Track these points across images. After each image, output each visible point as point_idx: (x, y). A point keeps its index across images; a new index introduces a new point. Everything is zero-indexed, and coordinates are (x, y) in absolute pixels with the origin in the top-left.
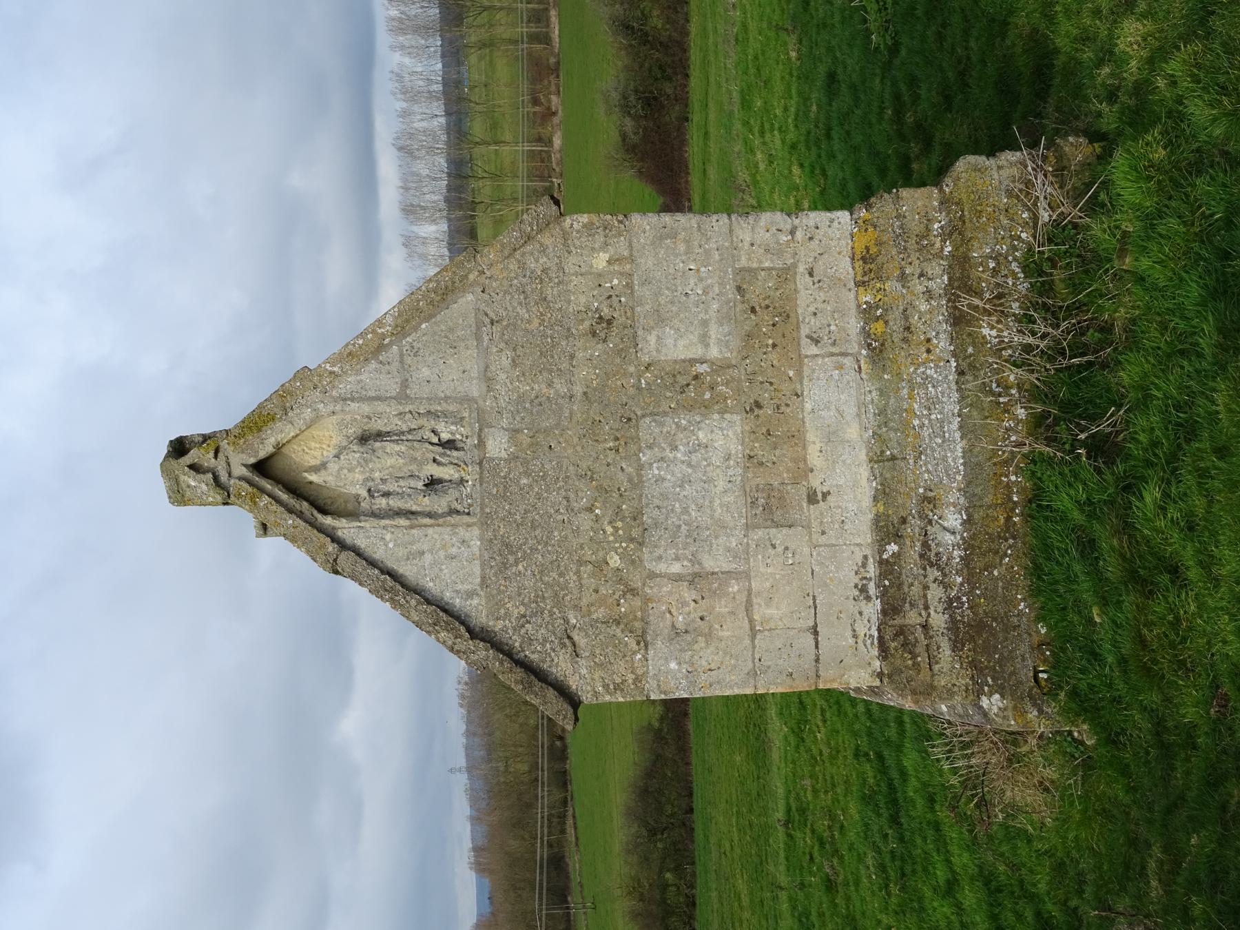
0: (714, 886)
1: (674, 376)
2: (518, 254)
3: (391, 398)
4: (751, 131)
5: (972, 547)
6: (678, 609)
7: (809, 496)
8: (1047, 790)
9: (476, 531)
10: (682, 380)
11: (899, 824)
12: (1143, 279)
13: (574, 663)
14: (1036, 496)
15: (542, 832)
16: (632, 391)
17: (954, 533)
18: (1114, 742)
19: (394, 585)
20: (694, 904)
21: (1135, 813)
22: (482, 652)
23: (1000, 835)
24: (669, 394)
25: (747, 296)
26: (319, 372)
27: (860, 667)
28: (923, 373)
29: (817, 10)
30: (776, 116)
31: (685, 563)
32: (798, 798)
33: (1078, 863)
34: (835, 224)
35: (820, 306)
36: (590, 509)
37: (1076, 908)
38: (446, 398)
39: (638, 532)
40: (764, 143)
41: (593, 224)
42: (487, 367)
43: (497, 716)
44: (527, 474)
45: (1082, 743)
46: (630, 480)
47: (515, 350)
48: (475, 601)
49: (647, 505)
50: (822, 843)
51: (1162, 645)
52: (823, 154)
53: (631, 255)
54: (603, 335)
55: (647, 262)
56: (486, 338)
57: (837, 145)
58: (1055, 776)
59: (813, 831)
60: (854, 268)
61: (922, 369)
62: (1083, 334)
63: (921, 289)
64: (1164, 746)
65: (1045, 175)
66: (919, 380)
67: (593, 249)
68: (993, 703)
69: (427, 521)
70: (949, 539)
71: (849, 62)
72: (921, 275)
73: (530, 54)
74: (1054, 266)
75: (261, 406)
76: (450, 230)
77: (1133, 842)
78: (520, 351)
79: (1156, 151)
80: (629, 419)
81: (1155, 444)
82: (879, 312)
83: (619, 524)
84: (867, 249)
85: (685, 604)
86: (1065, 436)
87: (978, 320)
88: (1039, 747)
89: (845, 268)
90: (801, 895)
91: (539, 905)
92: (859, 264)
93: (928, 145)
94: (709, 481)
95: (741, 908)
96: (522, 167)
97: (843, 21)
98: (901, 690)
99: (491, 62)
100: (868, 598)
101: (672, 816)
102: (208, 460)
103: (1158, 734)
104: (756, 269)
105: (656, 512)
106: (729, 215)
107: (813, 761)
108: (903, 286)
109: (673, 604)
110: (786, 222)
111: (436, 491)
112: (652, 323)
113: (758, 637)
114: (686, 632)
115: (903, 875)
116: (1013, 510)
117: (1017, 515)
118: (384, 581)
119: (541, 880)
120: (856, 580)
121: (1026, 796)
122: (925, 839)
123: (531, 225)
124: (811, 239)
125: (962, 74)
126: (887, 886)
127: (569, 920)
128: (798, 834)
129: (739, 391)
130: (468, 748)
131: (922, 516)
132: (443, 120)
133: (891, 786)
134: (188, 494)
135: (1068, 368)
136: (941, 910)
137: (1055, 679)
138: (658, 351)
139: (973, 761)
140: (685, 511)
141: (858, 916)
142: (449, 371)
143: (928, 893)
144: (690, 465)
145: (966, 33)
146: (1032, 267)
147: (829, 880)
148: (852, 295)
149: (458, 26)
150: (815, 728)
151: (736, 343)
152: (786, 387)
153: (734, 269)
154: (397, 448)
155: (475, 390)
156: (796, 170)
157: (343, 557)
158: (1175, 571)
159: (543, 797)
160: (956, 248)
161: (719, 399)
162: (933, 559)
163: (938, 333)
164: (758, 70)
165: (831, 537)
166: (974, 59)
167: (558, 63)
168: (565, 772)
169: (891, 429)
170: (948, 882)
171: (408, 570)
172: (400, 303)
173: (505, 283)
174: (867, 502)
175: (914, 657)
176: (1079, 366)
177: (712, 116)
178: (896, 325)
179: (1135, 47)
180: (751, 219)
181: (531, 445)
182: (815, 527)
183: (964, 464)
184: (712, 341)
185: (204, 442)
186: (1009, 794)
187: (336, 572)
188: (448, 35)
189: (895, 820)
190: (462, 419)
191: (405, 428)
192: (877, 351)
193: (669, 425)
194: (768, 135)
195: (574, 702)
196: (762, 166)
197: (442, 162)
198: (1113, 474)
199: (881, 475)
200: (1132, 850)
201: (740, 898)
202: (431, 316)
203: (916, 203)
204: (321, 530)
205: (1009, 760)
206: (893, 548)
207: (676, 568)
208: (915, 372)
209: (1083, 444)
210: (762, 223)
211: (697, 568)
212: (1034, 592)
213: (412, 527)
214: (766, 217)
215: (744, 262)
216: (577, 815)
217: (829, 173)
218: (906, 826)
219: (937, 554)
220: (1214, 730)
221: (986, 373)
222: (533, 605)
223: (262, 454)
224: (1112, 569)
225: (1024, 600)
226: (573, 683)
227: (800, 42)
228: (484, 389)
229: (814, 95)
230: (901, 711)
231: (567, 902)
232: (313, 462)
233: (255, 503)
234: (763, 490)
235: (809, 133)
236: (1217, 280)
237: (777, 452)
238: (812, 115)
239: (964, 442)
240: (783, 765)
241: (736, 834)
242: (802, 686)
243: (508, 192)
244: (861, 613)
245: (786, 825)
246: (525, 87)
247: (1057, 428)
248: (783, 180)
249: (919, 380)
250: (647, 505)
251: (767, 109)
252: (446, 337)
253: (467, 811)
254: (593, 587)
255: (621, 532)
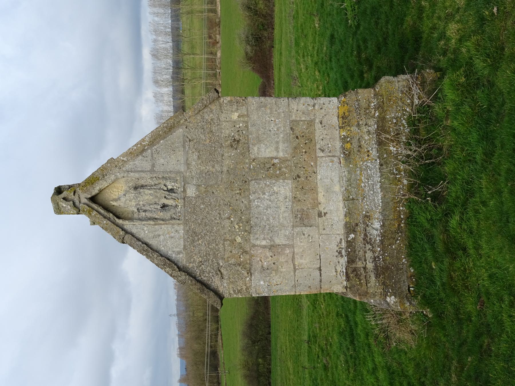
0: (279, 365)
1: (264, 164)
2: (201, 113)
3: (147, 171)
4: (299, 55)
5: (384, 236)
6: (264, 260)
7: (318, 214)
8: (413, 334)
9: (182, 227)
10: (268, 166)
11: (354, 344)
12: (455, 130)
13: (221, 281)
14: (410, 216)
15: (208, 342)
16: (247, 170)
17: (377, 230)
18: (439, 316)
19: (147, 249)
20: (270, 372)
21: (447, 345)
22: (183, 277)
23: (394, 350)
24: (262, 171)
25: (295, 132)
26: (118, 160)
27: (338, 284)
28: (366, 165)
29: (327, 8)
30: (309, 50)
31: (268, 241)
32: (313, 332)
33: (425, 363)
34: (331, 103)
35: (325, 136)
36: (229, 218)
37: (424, 382)
38: (170, 172)
39: (248, 227)
40: (304, 61)
41: (232, 101)
42: (188, 159)
43: (189, 294)
44: (203, 203)
45: (427, 316)
46: (246, 207)
47: (199, 152)
48: (181, 256)
49: (252, 217)
50: (323, 351)
51: (459, 279)
52: (328, 67)
53: (248, 114)
54: (235, 147)
55: (254, 117)
56: (187, 147)
57: (334, 64)
58: (417, 329)
59: (319, 345)
60: (338, 121)
61: (365, 163)
62: (431, 150)
63: (366, 130)
64: (460, 320)
65: (417, 85)
66: (364, 167)
67: (232, 111)
68: (391, 300)
69: (162, 222)
70: (375, 232)
71: (340, 30)
72: (366, 125)
73: (208, 17)
74: (419, 122)
75: (93, 174)
76: (173, 90)
77: (447, 357)
78: (201, 153)
79: (461, 79)
80: (246, 182)
81: (458, 197)
82: (348, 139)
83: (241, 225)
84: (344, 113)
85: (267, 258)
86: (422, 192)
87: (388, 143)
88: (410, 317)
89: (335, 121)
90: (314, 372)
91: (206, 372)
92: (341, 119)
93: (371, 67)
94: (278, 207)
95: (290, 374)
96: (204, 65)
97: (337, 13)
98: (354, 294)
99: (192, 20)
100: (342, 256)
101: (262, 335)
102: (71, 196)
103: (457, 314)
104: (299, 121)
105: (256, 220)
106: (288, 98)
107: (320, 317)
108: (359, 129)
109: (262, 258)
110: (311, 102)
111: (166, 210)
112: (256, 142)
113: (297, 271)
114: (268, 269)
115: (355, 365)
116: (401, 221)
117: (403, 223)
118: (144, 247)
119: (207, 361)
120: (337, 249)
121: (405, 336)
122: (364, 350)
123: (206, 101)
124: (321, 109)
125: (385, 39)
126: (348, 369)
127: (218, 378)
128: (313, 347)
129: (291, 171)
130: (177, 306)
131: (365, 223)
132: (171, 44)
133: (351, 329)
134: (62, 210)
135: (425, 164)
136: (370, 379)
137: (417, 290)
138: (258, 154)
139: (384, 321)
140: (268, 219)
141: (337, 381)
142: (171, 160)
143: (365, 373)
144: (270, 201)
145: (387, 22)
146: (411, 122)
147: (325, 366)
148: (338, 132)
149: (178, 5)
150: (320, 303)
151: (290, 151)
152: (310, 169)
153: (290, 121)
154: (150, 192)
155: (182, 168)
156: (317, 73)
157: (126, 237)
158: (464, 250)
159: (208, 327)
160: (380, 114)
161: (282, 174)
162: (368, 240)
163: (372, 149)
164: (302, 30)
165: (327, 231)
166: (390, 33)
167: (220, 21)
168: (218, 317)
169: (353, 187)
170: (373, 369)
171: (153, 243)
172: (152, 132)
173: (196, 124)
174: (342, 217)
175: (360, 280)
176: (429, 163)
177: (283, 46)
178: (355, 145)
179: (454, 34)
180: (297, 100)
181: (205, 191)
182: (321, 227)
183: (382, 202)
184: (280, 150)
185: (69, 188)
186: (398, 335)
187: (124, 243)
188: (174, 8)
189: (352, 342)
190: (177, 180)
191: (153, 184)
192: (348, 155)
193: (262, 183)
194: (306, 58)
195: (221, 298)
196: (303, 70)
197: (170, 61)
198: (441, 208)
199: (348, 206)
200: (446, 360)
201: (289, 370)
202: (165, 138)
203: (364, 94)
204: (117, 225)
205: (398, 322)
206: (352, 236)
207: (264, 243)
208: (362, 164)
209: (430, 196)
210: (302, 102)
211: (272, 243)
212: (409, 255)
213: (155, 225)
214: (303, 99)
215: (294, 118)
216: (223, 334)
217: (331, 76)
218: (356, 345)
219: (370, 239)
220: (478, 315)
221: (391, 165)
222: (205, 257)
223: (94, 194)
224: (440, 248)
225: (405, 258)
226: (221, 290)
227: (320, 20)
228: (186, 168)
229: (325, 43)
230: (355, 302)
231: (218, 370)
232: (115, 197)
233: (90, 214)
234: (300, 211)
235: (323, 58)
236: (484, 132)
237: (306, 196)
238: (324, 51)
239: (382, 193)
240: (307, 317)
241: (288, 344)
242: (314, 291)
243: (198, 75)
244: (339, 262)
245: (308, 342)
246: (205, 31)
247: (419, 189)
248: (312, 77)
249: (364, 167)
250: (252, 217)
251: (305, 47)
252: (171, 146)
253: (177, 332)
254: (230, 250)
255: (241, 228)
